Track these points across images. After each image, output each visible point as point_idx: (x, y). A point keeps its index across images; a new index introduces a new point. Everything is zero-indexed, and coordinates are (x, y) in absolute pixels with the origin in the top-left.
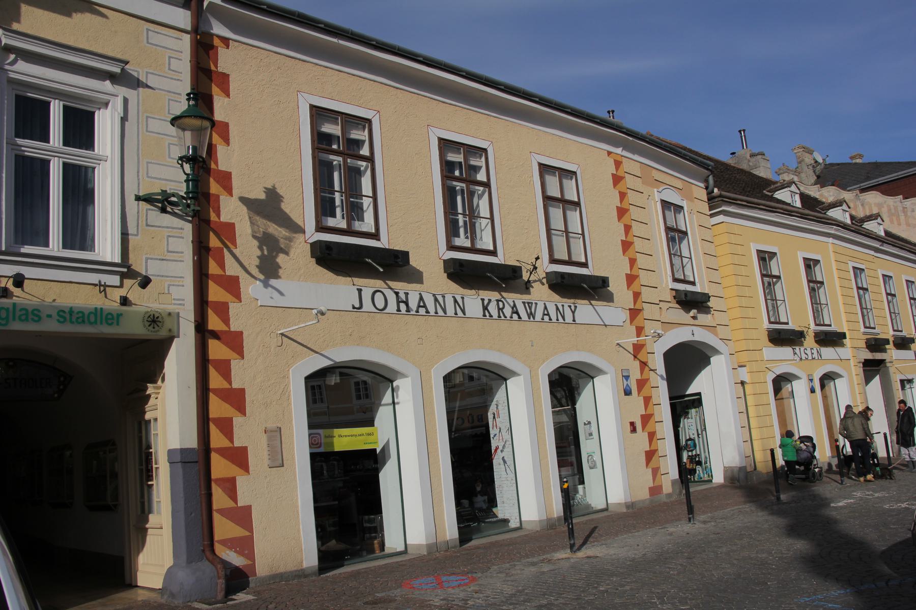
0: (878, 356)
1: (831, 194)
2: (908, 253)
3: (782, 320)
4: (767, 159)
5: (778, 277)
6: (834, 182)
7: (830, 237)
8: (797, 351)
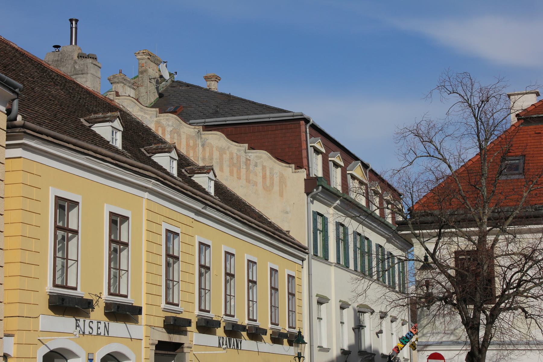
0: (176, 338)
1: (170, 123)
2: (233, 220)
3: (69, 284)
4: (99, 65)
5: (76, 232)
6: (177, 107)
7: (146, 191)
8: (81, 323)
